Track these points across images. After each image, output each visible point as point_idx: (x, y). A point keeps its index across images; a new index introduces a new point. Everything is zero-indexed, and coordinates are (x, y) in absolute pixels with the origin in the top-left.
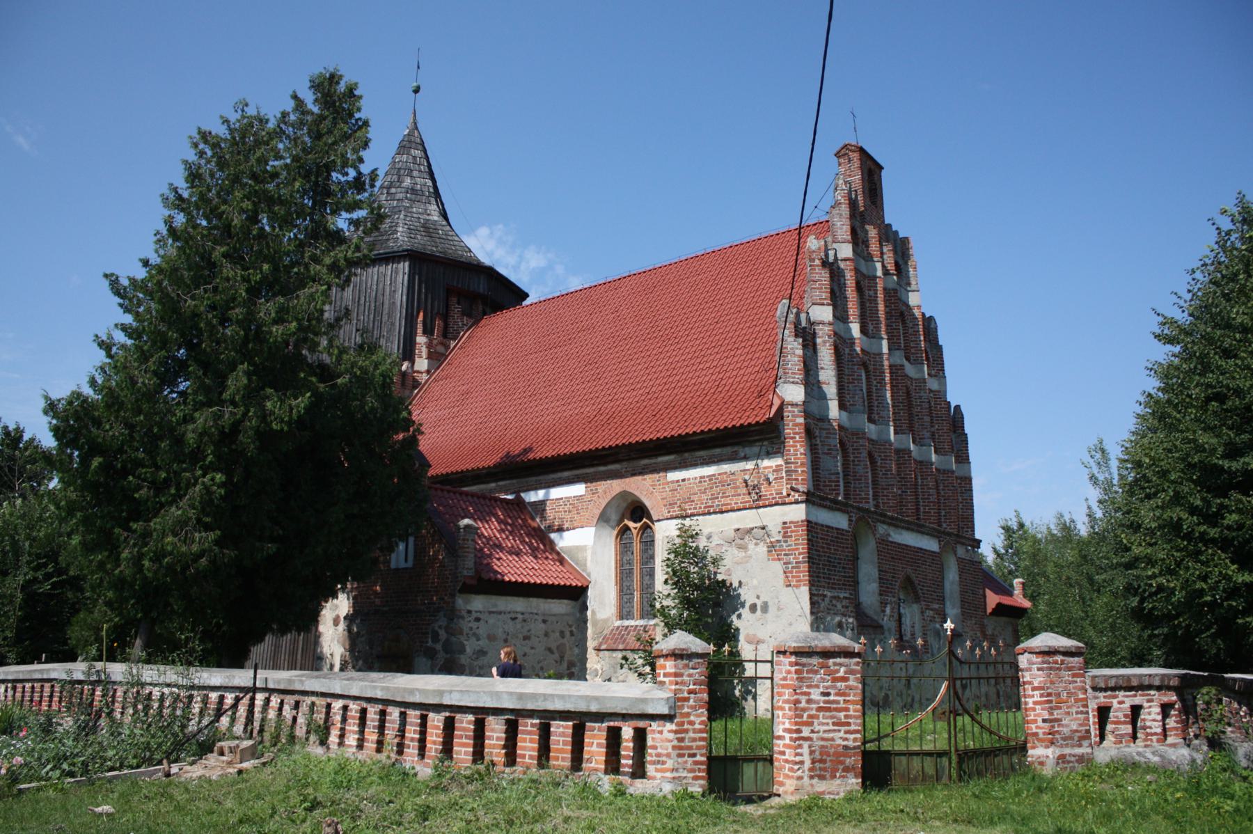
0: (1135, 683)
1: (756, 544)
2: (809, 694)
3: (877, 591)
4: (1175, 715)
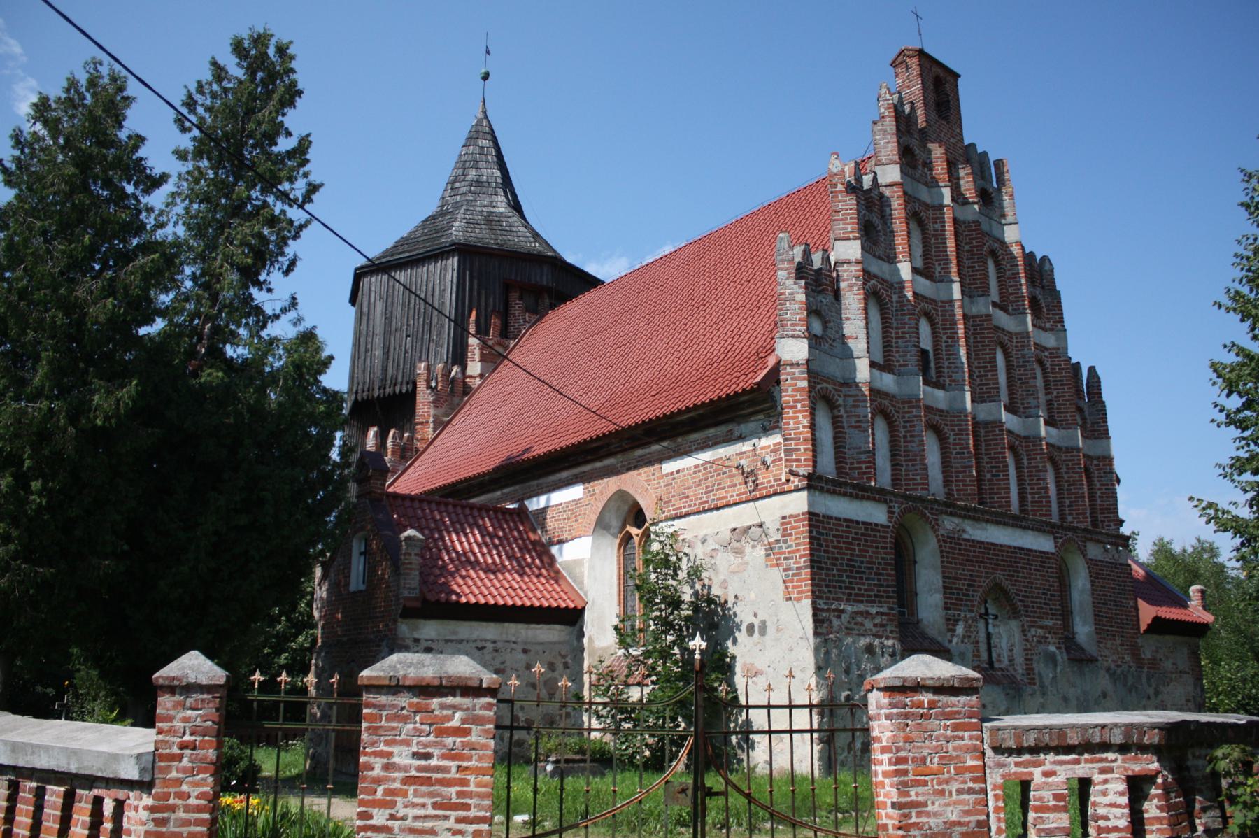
0: (1074, 739)
1: (753, 547)
2: (390, 754)
3: (941, 604)
4: (1157, 796)
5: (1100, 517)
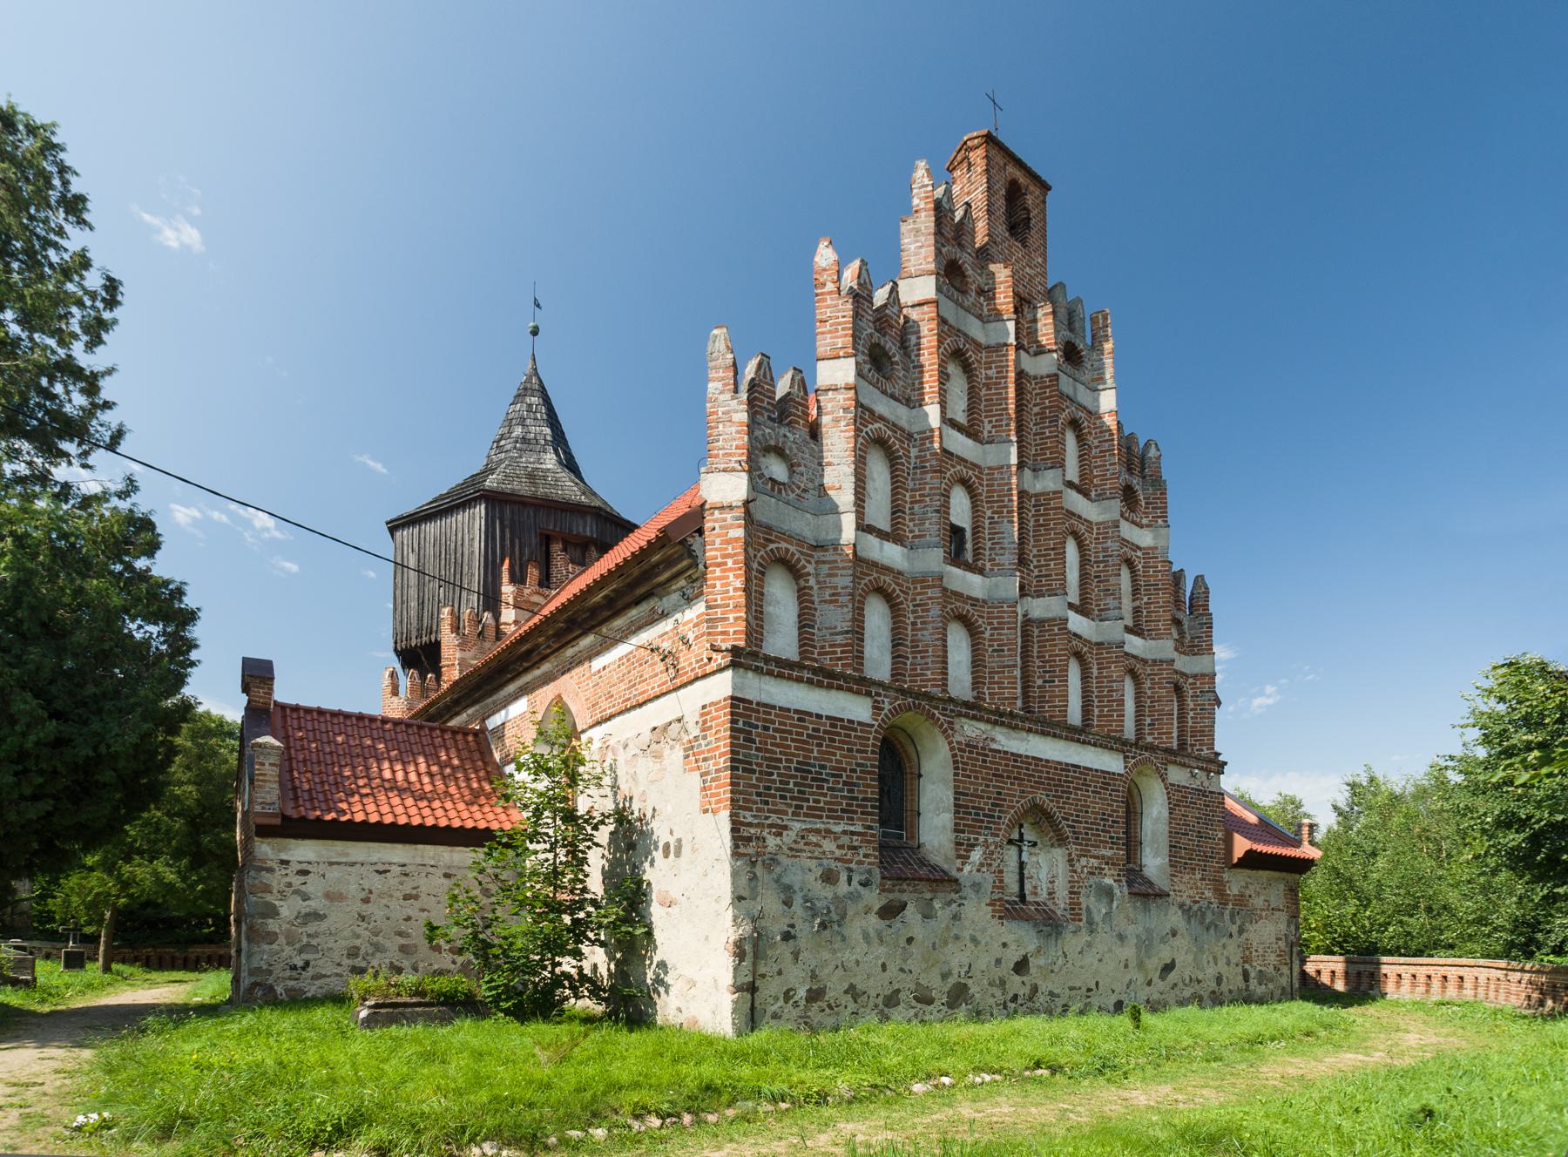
3: (950, 825)
5: (1190, 741)
